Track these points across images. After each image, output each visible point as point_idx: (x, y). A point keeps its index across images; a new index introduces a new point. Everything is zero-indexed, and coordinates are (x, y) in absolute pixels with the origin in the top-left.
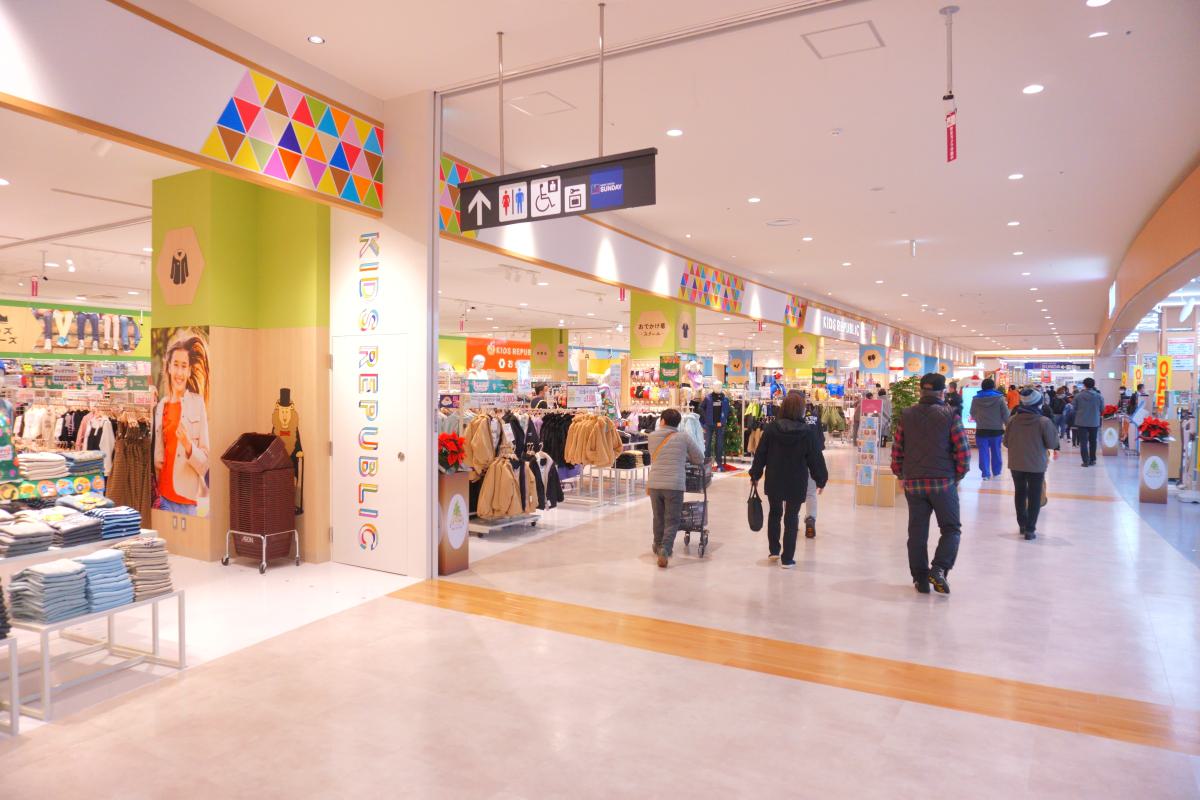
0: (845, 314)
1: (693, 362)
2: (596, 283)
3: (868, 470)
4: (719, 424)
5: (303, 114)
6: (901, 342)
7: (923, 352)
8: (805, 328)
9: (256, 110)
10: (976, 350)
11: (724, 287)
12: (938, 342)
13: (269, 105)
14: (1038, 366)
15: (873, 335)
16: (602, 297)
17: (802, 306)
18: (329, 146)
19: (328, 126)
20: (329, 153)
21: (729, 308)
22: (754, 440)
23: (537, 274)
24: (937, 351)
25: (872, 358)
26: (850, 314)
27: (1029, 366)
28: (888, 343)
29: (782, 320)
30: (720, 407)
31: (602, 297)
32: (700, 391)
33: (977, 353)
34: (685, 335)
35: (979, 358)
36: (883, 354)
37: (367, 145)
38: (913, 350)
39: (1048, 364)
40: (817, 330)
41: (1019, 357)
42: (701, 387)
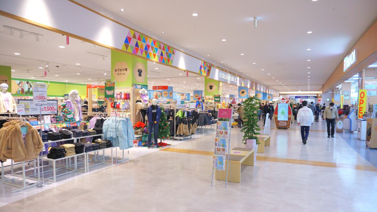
0: (230, 73)
1: (143, 89)
2: (150, 62)
3: (221, 159)
4: (155, 122)
5: (139, 39)
6: (254, 87)
7: (262, 91)
8: (210, 77)
9: (131, 38)
10: (280, 91)
11: (160, 51)
12: (267, 87)
13: (133, 37)
14: (299, 97)
15: (243, 83)
16: (105, 57)
17: (209, 67)
18: (144, 45)
19: (144, 41)
20: (144, 48)
21: (164, 62)
22: (180, 128)
23: (39, 36)
24: (267, 91)
25: (243, 92)
26: (233, 73)
27: (296, 97)
28: (249, 86)
29: (198, 71)
30: (156, 113)
31: (105, 57)
32: (147, 104)
33: (280, 93)
34: (140, 75)
35: (281, 94)
36: (247, 91)
37: (151, 45)
38: (258, 90)
39: (302, 97)
40: (216, 78)
41: (293, 94)
42: (148, 102)
